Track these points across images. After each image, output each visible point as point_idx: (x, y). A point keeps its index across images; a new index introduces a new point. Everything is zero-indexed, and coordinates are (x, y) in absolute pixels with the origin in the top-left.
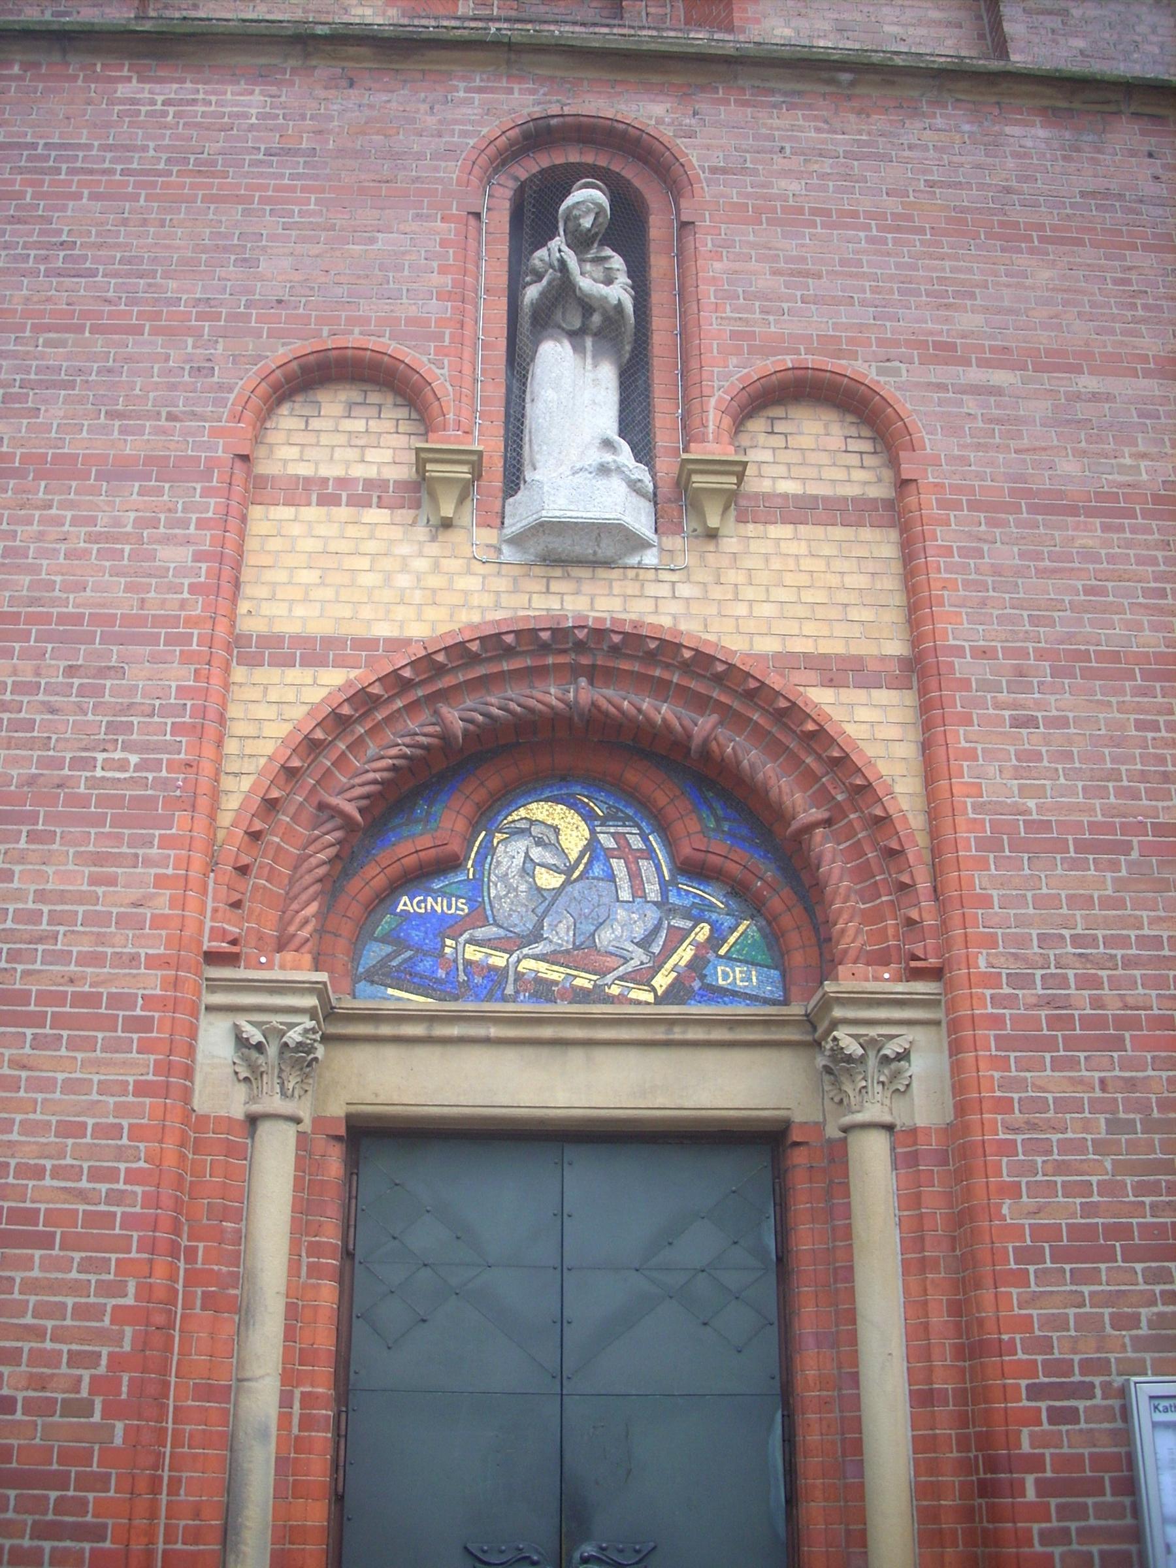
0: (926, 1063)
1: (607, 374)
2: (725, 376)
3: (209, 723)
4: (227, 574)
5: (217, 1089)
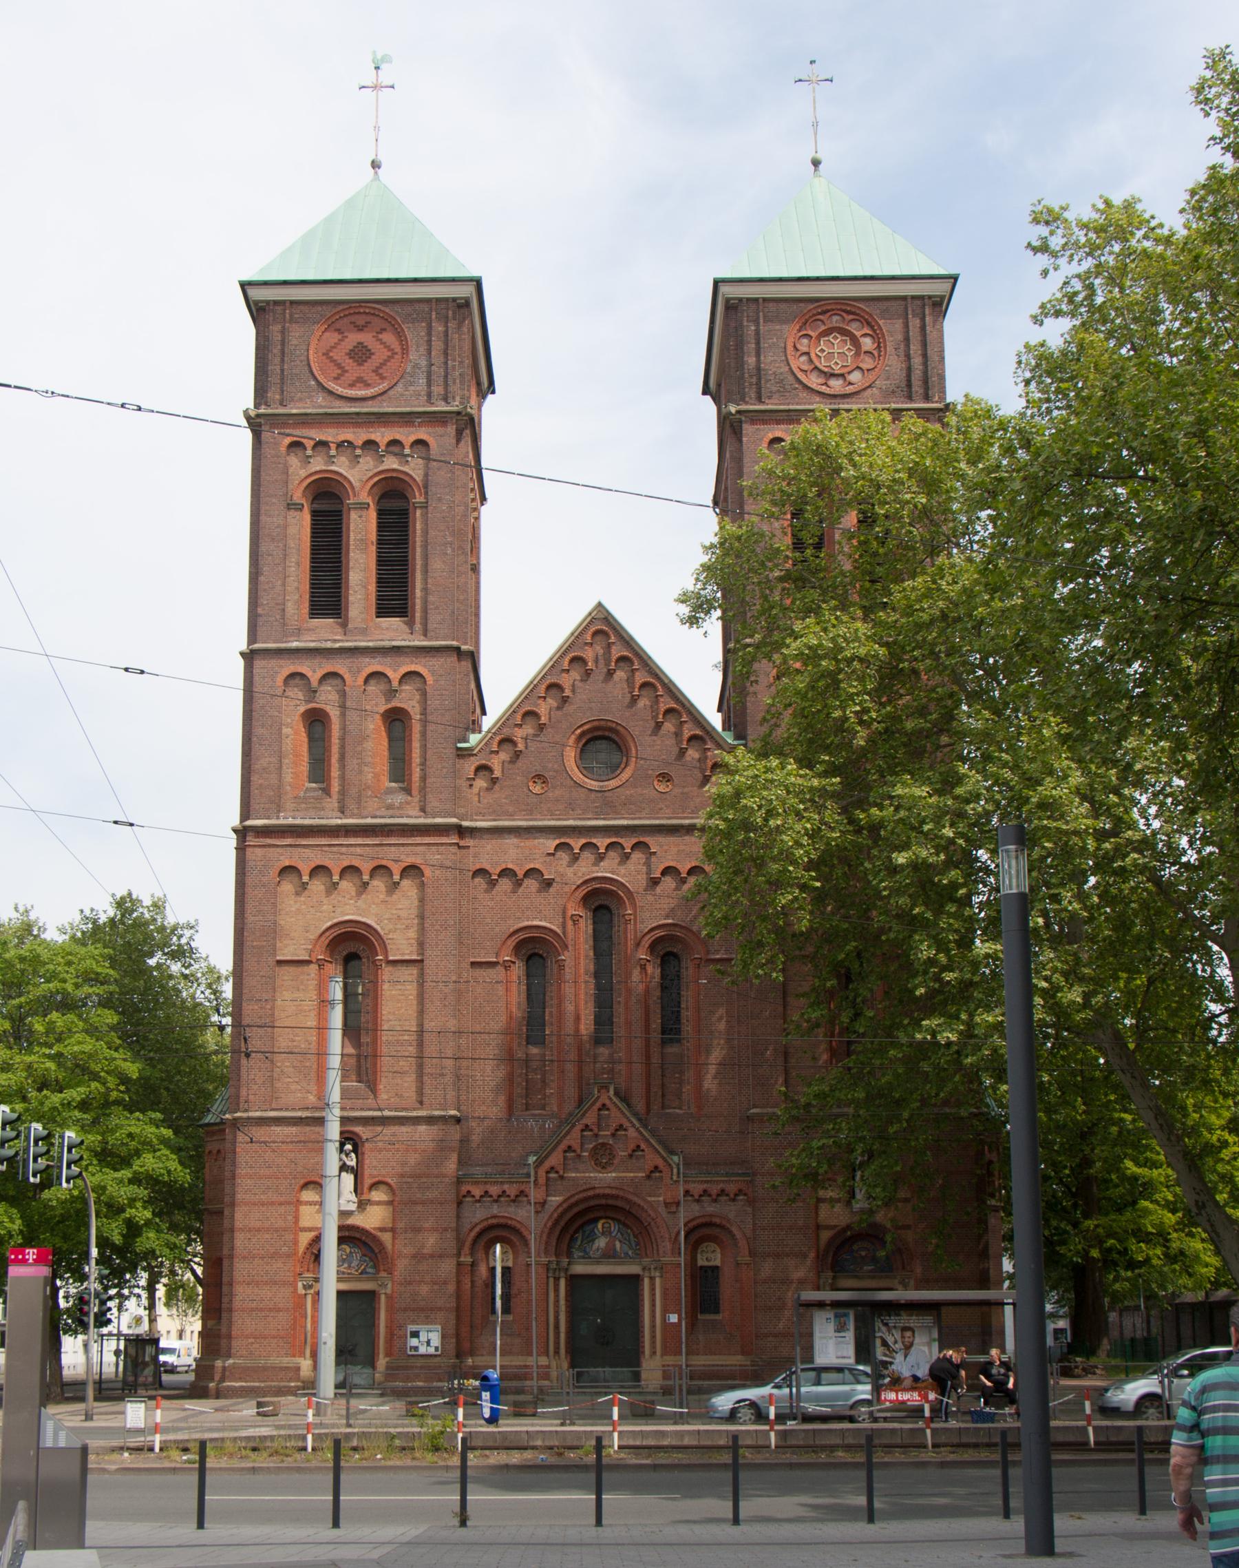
0: (389, 1286)
1: (352, 1177)
2: (368, 1182)
3: (296, 1242)
4: (297, 1219)
5: (301, 1291)
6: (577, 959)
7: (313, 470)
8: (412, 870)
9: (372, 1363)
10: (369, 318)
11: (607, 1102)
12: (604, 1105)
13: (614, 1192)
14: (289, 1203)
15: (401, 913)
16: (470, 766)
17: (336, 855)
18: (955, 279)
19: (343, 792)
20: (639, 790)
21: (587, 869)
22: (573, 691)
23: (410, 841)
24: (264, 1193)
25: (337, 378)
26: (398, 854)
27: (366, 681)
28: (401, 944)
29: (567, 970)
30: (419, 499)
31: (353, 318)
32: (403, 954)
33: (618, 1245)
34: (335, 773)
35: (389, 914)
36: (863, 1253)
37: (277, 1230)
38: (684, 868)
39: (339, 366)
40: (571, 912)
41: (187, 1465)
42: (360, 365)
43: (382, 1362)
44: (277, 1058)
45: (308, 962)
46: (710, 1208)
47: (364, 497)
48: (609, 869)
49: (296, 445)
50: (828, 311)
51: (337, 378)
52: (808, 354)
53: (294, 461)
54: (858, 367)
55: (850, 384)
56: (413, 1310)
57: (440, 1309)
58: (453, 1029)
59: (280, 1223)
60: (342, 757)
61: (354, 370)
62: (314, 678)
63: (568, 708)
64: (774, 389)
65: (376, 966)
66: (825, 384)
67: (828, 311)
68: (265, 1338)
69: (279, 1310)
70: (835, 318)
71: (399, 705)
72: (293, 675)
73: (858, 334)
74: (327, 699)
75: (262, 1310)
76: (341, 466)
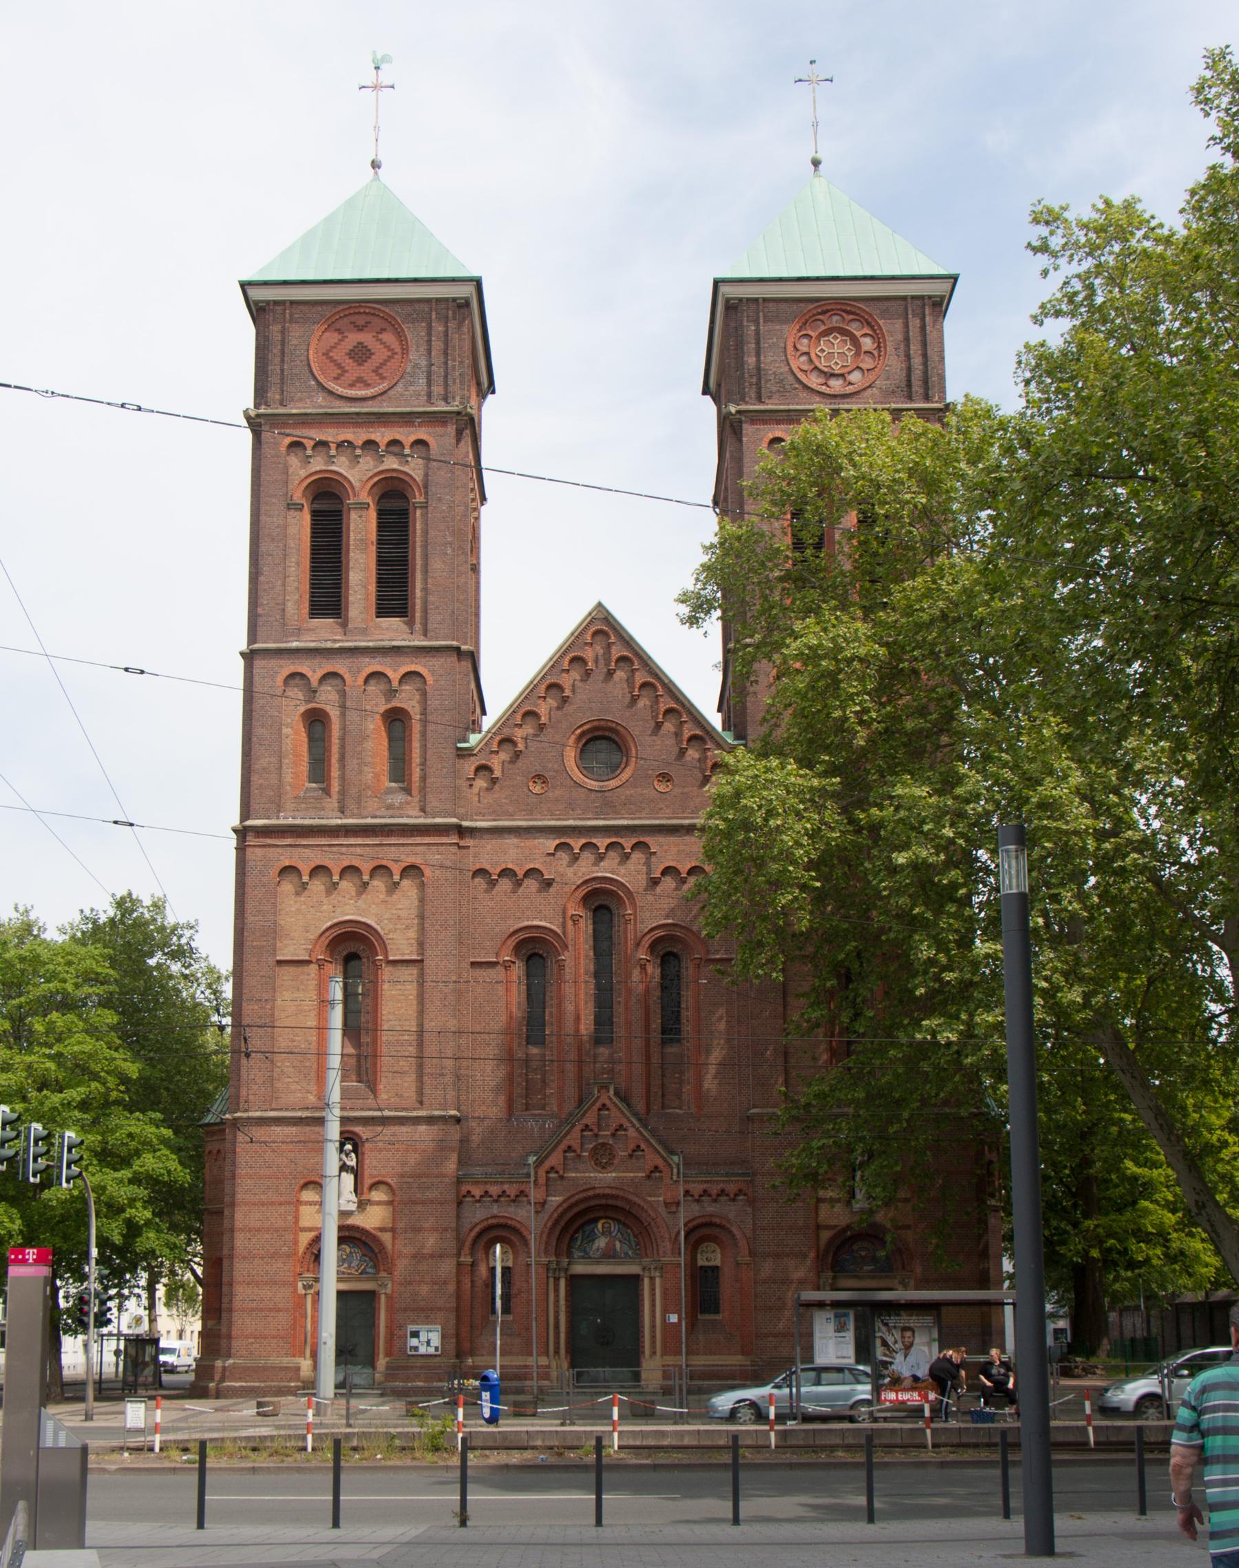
0: (389, 1286)
1: (352, 1177)
2: (368, 1182)
3: (296, 1242)
4: (297, 1219)
5: (301, 1291)
6: (577, 959)
7: (313, 470)
8: (412, 870)
9: (372, 1363)
10: (369, 318)
11: (607, 1102)
12: (604, 1105)
13: (614, 1192)
14: (289, 1203)
15: (401, 913)
16: (470, 766)
17: (336, 855)
18: (955, 279)
19: (343, 792)
20: (639, 790)
21: (587, 869)
22: (573, 691)
23: (410, 841)
24: (264, 1193)
25: (337, 378)
26: (398, 854)
27: (366, 681)
28: (401, 944)
29: (567, 970)
30: (419, 499)
31: (353, 318)
32: (403, 954)
33: (618, 1245)
34: (335, 773)
35: (389, 914)
36: (863, 1253)
37: (277, 1230)
38: (684, 868)
39: (339, 366)
40: (571, 912)
41: (187, 1465)
42: (360, 365)
43: (382, 1362)
44: (277, 1058)
45: (308, 962)
46: (710, 1208)
47: (364, 497)
48: (609, 869)
49: (296, 445)
50: (828, 311)
51: (337, 378)
52: (808, 354)
53: (294, 461)
54: (858, 367)
55: (850, 384)
56: (413, 1310)
57: (440, 1309)
58: (453, 1029)
59: (280, 1223)
60: (342, 757)
61: (354, 370)
62: (314, 678)
63: (568, 708)
64: (774, 389)
65: (376, 966)
66: (825, 384)
67: (828, 311)
68: (265, 1338)
69: (279, 1310)
70: (835, 318)
71: (399, 705)
72: (293, 675)
73: (858, 334)
74: (327, 699)
75: (262, 1310)
76: (341, 466)
